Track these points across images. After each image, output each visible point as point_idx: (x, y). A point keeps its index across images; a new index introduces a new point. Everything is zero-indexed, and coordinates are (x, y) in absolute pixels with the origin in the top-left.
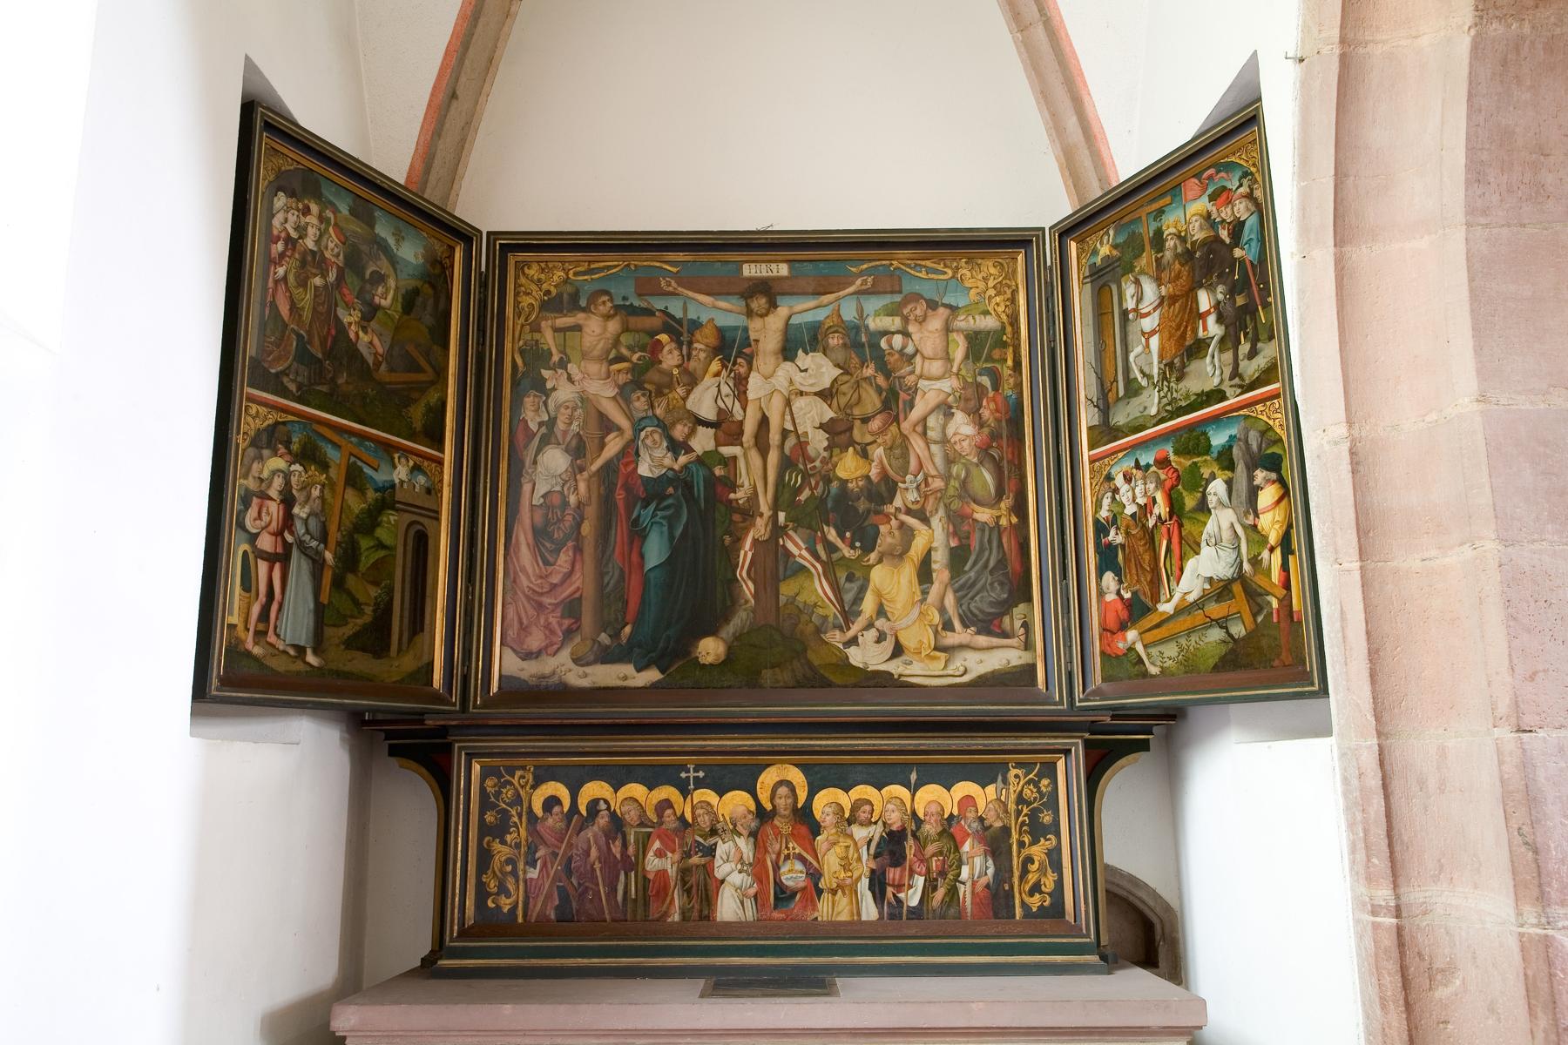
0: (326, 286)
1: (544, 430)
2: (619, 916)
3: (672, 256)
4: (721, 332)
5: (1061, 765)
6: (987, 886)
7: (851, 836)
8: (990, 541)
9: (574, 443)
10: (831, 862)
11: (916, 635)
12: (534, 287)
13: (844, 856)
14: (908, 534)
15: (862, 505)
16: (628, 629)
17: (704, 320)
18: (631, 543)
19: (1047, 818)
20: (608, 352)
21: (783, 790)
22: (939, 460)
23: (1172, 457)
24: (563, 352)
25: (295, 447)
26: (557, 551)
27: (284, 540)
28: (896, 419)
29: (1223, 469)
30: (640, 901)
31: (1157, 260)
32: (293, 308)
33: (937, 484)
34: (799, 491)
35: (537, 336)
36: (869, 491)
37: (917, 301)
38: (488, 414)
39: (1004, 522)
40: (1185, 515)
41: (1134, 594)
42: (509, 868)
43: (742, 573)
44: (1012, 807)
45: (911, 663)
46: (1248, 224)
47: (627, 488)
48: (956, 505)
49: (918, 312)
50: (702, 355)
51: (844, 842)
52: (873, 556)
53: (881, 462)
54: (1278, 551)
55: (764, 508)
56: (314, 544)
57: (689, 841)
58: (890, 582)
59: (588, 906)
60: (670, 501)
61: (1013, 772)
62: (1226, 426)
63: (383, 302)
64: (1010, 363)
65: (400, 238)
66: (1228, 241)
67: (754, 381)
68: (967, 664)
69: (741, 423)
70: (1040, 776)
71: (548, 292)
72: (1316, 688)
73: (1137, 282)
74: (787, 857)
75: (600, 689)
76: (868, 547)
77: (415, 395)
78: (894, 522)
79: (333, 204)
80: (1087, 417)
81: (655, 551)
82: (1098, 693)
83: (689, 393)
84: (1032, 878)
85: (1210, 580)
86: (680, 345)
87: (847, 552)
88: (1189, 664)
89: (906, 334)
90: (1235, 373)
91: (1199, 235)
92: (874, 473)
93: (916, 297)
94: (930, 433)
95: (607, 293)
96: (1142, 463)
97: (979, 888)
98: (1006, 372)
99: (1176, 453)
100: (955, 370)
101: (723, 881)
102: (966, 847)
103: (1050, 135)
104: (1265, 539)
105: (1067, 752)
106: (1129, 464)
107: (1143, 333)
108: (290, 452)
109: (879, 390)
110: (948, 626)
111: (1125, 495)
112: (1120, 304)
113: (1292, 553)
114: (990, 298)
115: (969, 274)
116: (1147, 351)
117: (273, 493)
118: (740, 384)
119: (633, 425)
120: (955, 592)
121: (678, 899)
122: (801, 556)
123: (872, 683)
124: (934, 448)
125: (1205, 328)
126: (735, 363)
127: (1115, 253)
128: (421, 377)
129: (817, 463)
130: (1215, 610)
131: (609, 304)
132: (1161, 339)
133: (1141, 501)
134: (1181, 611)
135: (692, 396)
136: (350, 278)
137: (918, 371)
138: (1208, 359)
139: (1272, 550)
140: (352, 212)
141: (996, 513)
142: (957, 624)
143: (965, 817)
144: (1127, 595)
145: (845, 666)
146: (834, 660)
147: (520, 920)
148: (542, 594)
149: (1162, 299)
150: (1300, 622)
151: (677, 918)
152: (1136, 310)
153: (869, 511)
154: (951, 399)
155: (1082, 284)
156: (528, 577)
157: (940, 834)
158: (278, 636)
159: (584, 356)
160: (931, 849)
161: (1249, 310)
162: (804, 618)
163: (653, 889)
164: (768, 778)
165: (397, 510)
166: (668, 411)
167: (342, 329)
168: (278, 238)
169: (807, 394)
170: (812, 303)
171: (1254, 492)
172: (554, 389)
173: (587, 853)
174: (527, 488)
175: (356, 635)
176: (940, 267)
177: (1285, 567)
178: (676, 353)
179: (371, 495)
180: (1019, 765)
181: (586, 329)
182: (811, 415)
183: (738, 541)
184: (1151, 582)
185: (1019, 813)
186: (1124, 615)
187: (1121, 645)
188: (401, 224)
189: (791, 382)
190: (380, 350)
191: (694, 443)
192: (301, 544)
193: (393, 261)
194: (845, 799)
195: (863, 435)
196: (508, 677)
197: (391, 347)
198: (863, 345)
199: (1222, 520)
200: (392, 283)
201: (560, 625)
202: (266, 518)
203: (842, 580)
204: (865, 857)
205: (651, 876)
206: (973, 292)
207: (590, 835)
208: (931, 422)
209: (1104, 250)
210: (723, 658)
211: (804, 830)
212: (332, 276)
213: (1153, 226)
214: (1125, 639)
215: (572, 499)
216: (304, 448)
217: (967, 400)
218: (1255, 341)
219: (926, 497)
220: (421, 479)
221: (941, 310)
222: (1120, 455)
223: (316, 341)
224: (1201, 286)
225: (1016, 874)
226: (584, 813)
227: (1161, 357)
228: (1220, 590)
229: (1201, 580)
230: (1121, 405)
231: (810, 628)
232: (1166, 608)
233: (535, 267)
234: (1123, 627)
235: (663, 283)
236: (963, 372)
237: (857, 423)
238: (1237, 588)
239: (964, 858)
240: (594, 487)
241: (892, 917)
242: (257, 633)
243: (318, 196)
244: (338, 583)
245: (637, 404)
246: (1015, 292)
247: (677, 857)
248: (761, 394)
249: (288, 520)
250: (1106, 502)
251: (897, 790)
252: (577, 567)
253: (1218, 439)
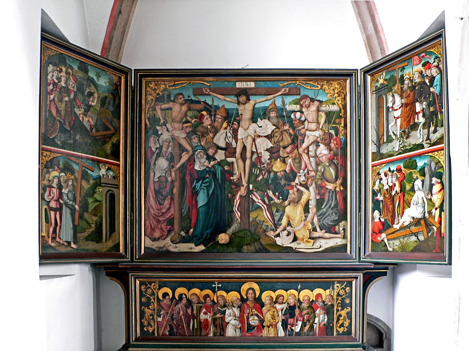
0: (70, 100)
1: (158, 151)
2: (191, 334)
3: (207, 78)
4: (227, 111)
5: (354, 283)
6: (324, 325)
7: (275, 308)
8: (332, 197)
9: (170, 156)
10: (268, 317)
11: (302, 233)
12: (153, 92)
13: (273, 314)
14: (300, 193)
15: (283, 182)
16: (192, 230)
17: (220, 106)
18: (192, 196)
19: (347, 301)
20: (182, 119)
21: (251, 291)
22: (313, 164)
23: (403, 169)
24: (165, 119)
25: (61, 166)
26: (165, 199)
27: (60, 203)
28: (297, 147)
29: (421, 176)
30: (199, 329)
31: (401, 88)
32: (58, 111)
33: (313, 174)
34: (258, 176)
35: (154, 112)
36: (286, 176)
37: (306, 99)
38: (136, 135)
39: (338, 189)
40: (406, 193)
41: (385, 220)
42: (151, 317)
43: (235, 209)
44: (335, 297)
45: (300, 244)
46: (436, 78)
47: (191, 175)
48: (320, 182)
49: (307, 103)
50: (220, 120)
51: (273, 310)
52: (287, 202)
53: (291, 165)
54: (438, 210)
55: (244, 183)
56: (71, 203)
57: (216, 309)
58: (293, 212)
59: (180, 331)
60: (207, 180)
61: (336, 285)
62: (424, 159)
63: (93, 104)
64: (342, 125)
65: (98, 76)
66: (428, 84)
67: (241, 132)
68: (321, 244)
69: (235, 148)
70: (346, 286)
71: (158, 94)
72: (447, 263)
73: (393, 96)
74: (252, 315)
75: (182, 252)
76: (285, 199)
77: (107, 140)
78: (295, 189)
79: (71, 66)
80: (372, 148)
81: (202, 200)
82: (369, 256)
83: (214, 136)
84: (341, 322)
85: (413, 218)
86: (211, 116)
87: (277, 201)
88: (403, 248)
89: (302, 112)
90: (428, 138)
91: (418, 80)
92: (288, 169)
93: (306, 97)
94: (310, 153)
95: (182, 94)
96: (392, 170)
97: (321, 325)
98: (341, 129)
99: (404, 167)
100: (321, 127)
101: (228, 323)
102: (318, 311)
103: (361, 31)
104: (434, 204)
105: (356, 278)
106: (386, 169)
107: (395, 117)
108: (59, 169)
109: (290, 135)
110: (315, 230)
111: (384, 181)
112: (386, 104)
113: (443, 211)
114: (335, 98)
115: (327, 87)
116: (395, 127)
117: (54, 185)
118: (235, 133)
119: (192, 149)
120: (318, 216)
121: (212, 329)
122: (258, 202)
123: (285, 251)
124: (311, 159)
125: (418, 119)
126: (233, 124)
127: (385, 83)
128: (109, 132)
129: (265, 165)
130: (413, 228)
131: (183, 99)
132: (401, 121)
133: (391, 184)
134: (402, 228)
135: (216, 137)
136: (80, 96)
137: (306, 128)
138: (418, 131)
139: (436, 209)
140: (79, 68)
141: (335, 185)
142: (318, 229)
143: (318, 301)
144: (383, 220)
145: (274, 244)
146: (270, 243)
147: (156, 335)
148: (159, 216)
149: (402, 104)
150: (444, 237)
151: (212, 335)
152: (392, 107)
153: (285, 184)
154: (319, 139)
155: (372, 94)
156: (153, 210)
157: (308, 307)
158: (60, 238)
159: (173, 120)
160: (305, 312)
161: (434, 114)
162: (259, 226)
163: (204, 325)
164: (245, 287)
165: (102, 186)
166: (206, 143)
167: (77, 117)
168: (50, 84)
169: (262, 137)
170: (264, 98)
171: (431, 186)
172: (161, 134)
173: (179, 313)
174: (152, 174)
175: (89, 235)
176: (316, 84)
177: (440, 216)
178: (209, 119)
179: (92, 182)
180: (339, 282)
181: (173, 109)
182: (263, 145)
183: (234, 196)
184: (392, 216)
185: (337, 299)
186: (381, 227)
187: (379, 239)
188: (99, 70)
189: (255, 132)
190: (92, 124)
191: (216, 157)
192: (66, 203)
193: (96, 86)
194: (274, 295)
195: (283, 154)
196: (147, 247)
197: (97, 121)
198: (284, 117)
199: (419, 195)
200: (96, 95)
201: (166, 228)
202: (52, 195)
203: (274, 212)
204: (280, 315)
205: (202, 321)
206: (329, 95)
207: (180, 306)
208: (311, 148)
209: (381, 81)
210: (228, 241)
211: (258, 305)
212: (72, 96)
213: (400, 74)
214: (381, 237)
215: (169, 179)
216: (64, 165)
217: (325, 140)
218: (436, 126)
219: (308, 179)
220: (111, 173)
221: (316, 102)
222: (384, 165)
223: (67, 124)
224: (417, 101)
225: (335, 320)
226: (177, 299)
227: (401, 128)
228: (416, 222)
229: (410, 217)
230: (385, 145)
231: (262, 230)
232: (397, 227)
233: (153, 83)
234: (380, 232)
235: (204, 90)
236: (324, 128)
237: (281, 149)
238: (422, 222)
239: (317, 315)
240: (178, 174)
241: (289, 335)
242: (52, 238)
243: (65, 64)
244: (81, 217)
245: (194, 140)
246: (345, 95)
247: (212, 314)
248: (243, 137)
249: (61, 195)
250: (377, 183)
251: (293, 291)
252: (172, 206)
253: (420, 163)
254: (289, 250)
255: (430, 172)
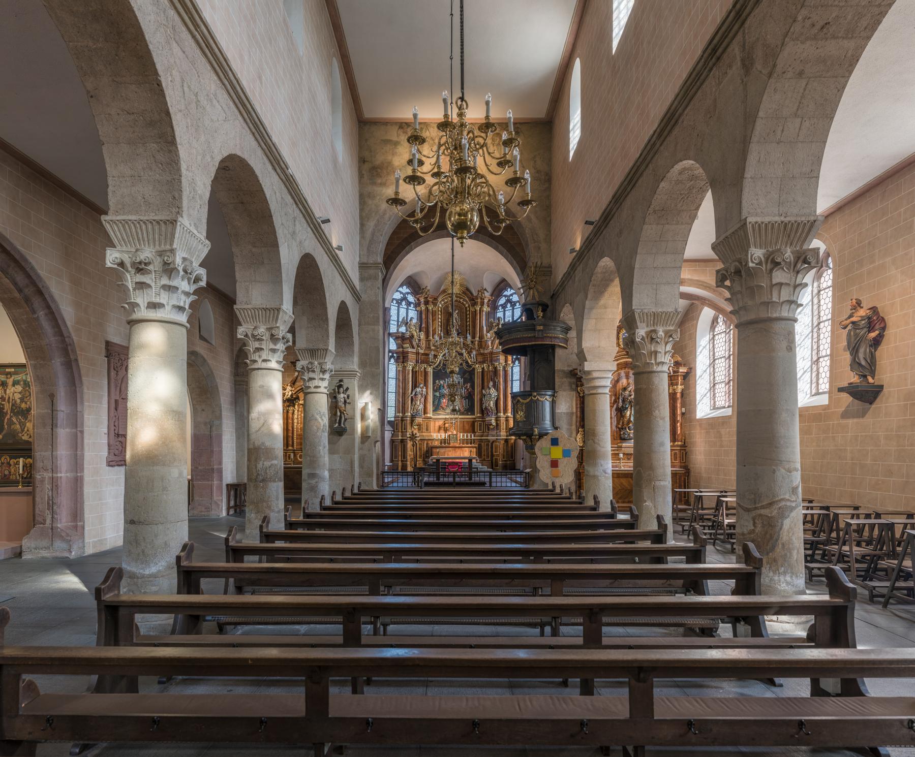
10: (13, 470)
118: (5, 391)
189: (462, 243)
254: (788, 500)
255: (79, 408)
